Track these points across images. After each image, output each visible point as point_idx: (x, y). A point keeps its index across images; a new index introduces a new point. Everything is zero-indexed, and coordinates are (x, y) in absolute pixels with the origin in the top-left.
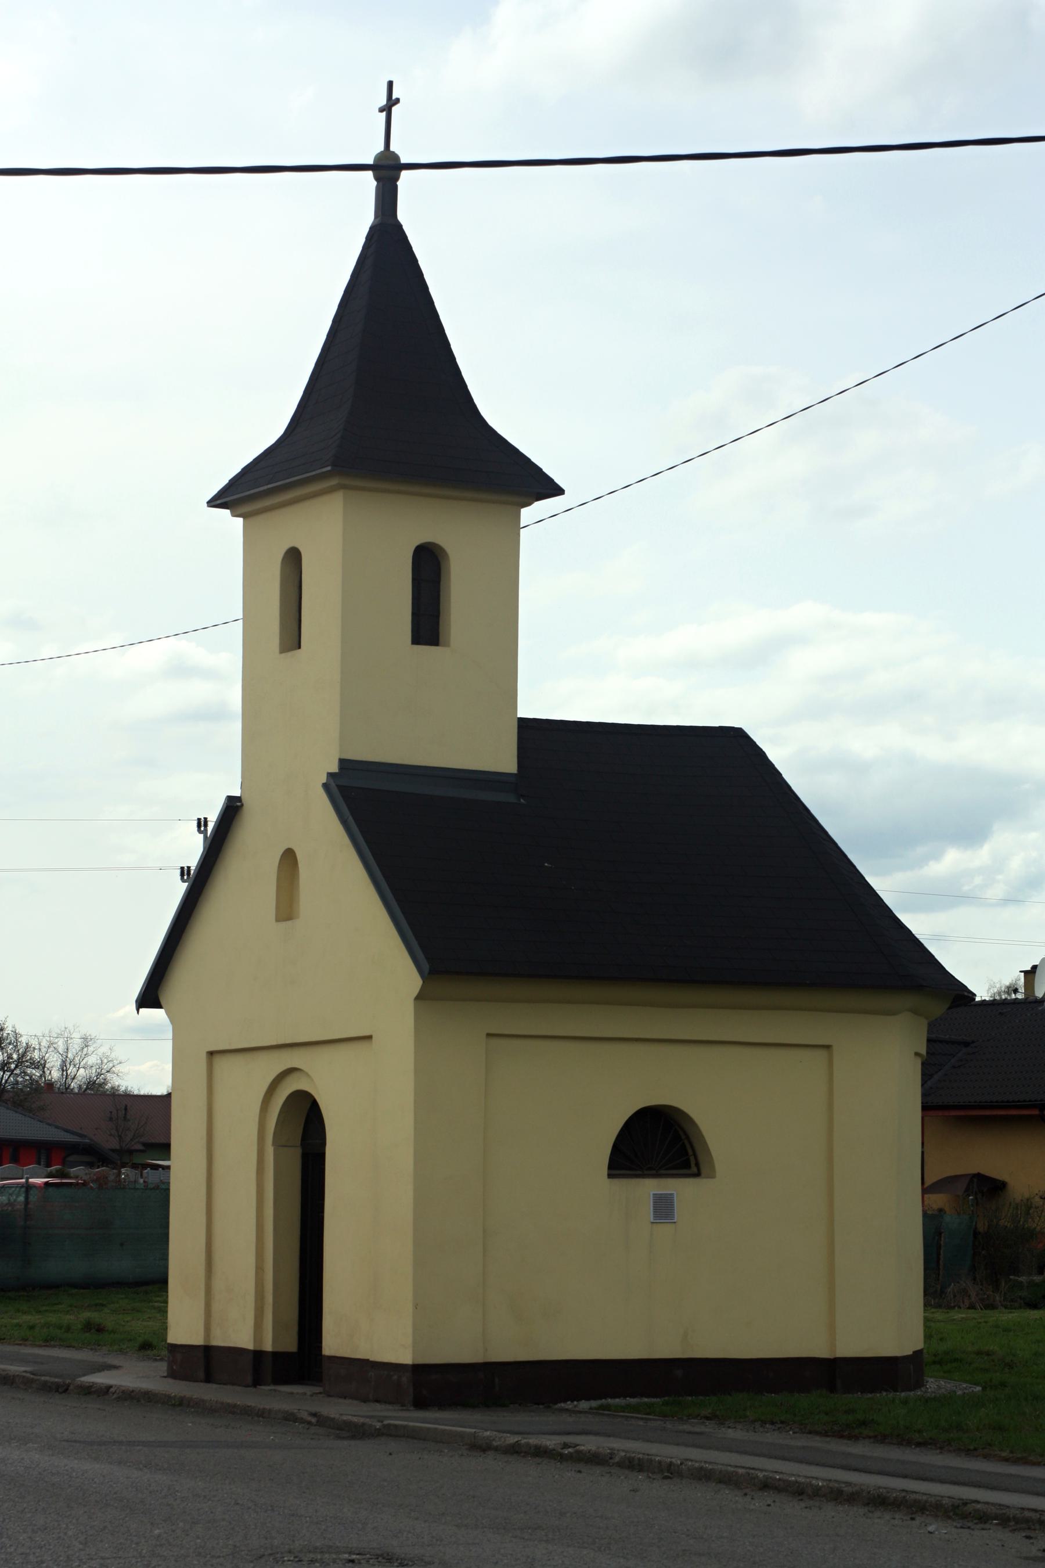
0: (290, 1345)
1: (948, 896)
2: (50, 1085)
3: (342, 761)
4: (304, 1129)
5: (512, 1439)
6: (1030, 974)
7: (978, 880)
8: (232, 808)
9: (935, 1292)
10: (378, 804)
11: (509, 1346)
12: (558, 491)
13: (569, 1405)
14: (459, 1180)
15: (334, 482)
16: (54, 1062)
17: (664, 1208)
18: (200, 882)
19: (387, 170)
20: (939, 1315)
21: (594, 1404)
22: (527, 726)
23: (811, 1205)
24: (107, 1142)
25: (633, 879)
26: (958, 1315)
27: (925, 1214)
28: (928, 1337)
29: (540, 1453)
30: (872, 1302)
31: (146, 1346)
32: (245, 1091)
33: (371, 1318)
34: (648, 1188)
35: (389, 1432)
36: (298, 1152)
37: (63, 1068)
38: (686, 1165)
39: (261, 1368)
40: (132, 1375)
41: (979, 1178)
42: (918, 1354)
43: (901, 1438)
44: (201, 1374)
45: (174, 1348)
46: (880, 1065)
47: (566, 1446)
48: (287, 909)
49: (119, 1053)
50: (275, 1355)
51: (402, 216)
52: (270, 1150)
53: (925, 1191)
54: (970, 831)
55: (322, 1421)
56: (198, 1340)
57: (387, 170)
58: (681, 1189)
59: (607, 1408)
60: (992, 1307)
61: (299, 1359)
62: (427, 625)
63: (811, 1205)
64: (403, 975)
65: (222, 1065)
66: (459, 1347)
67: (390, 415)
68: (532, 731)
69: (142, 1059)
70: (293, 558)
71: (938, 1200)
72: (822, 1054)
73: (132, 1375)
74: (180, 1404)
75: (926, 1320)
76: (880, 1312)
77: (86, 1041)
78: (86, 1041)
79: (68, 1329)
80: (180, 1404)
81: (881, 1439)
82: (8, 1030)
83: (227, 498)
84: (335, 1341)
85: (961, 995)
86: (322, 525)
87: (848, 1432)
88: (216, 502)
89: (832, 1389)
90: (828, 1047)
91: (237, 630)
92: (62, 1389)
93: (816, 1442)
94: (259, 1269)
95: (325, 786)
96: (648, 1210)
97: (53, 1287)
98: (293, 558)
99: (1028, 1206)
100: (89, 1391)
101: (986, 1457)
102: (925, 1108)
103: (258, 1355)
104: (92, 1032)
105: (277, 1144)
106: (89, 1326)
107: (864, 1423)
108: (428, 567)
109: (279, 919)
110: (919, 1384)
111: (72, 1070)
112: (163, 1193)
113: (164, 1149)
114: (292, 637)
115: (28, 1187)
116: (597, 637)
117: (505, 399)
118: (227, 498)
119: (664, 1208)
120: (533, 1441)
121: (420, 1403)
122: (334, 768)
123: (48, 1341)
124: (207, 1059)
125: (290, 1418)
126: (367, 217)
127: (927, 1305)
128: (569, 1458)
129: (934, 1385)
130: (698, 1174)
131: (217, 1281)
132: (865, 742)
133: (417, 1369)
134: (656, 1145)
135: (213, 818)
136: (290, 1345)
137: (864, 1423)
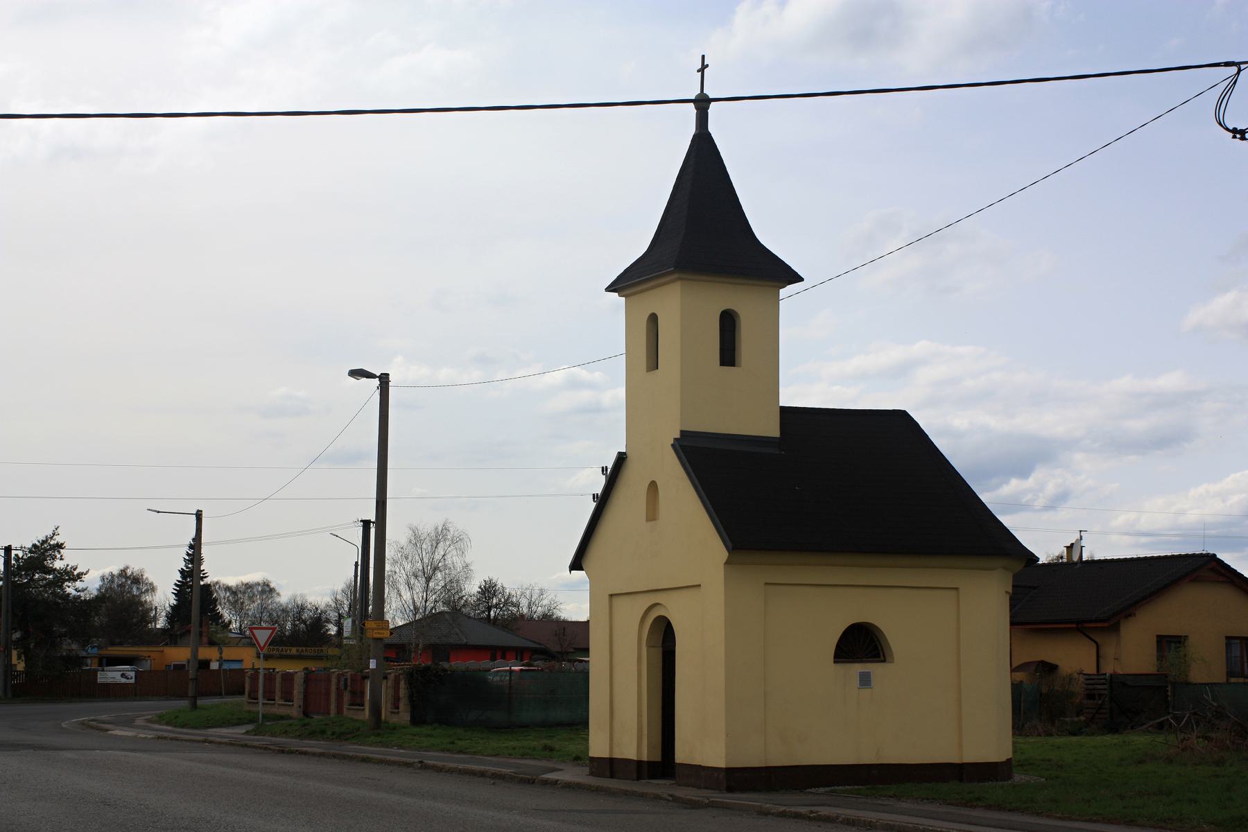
0: (657, 757)
1: (1016, 506)
2: (522, 616)
3: (682, 432)
4: (664, 638)
5: (782, 809)
6: (1070, 548)
7: (1029, 496)
8: (621, 459)
9: (1019, 727)
10: (704, 457)
11: (779, 757)
12: (800, 279)
13: (813, 790)
14: (753, 670)
15: (676, 276)
16: (524, 602)
17: (865, 680)
18: (603, 501)
19: (702, 103)
20: (1020, 740)
21: (827, 789)
22: (784, 410)
23: (948, 681)
24: (554, 648)
25: (847, 496)
26: (1031, 740)
27: (1012, 684)
28: (1014, 752)
29: (797, 816)
30: (987, 736)
31: (577, 758)
32: (630, 618)
33: (703, 742)
34: (857, 668)
35: (713, 805)
36: (660, 650)
37: (529, 607)
38: (878, 656)
39: (641, 770)
40: (569, 774)
41: (1043, 663)
42: (1009, 760)
43: (1000, 808)
44: (608, 774)
45: (592, 759)
46: (986, 599)
47: (812, 812)
48: (652, 515)
49: (560, 598)
50: (648, 762)
51: (712, 128)
52: (644, 649)
53: (1012, 671)
54: (1023, 471)
55: (676, 799)
56: (606, 755)
57: (702, 103)
58: (874, 669)
59: (835, 791)
60: (1051, 735)
61: (663, 765)
62: (728, 356)
63: (948, 681)
64: (718, 551)
65: (616, 601)
66: (752, 757)
67: (707, 241)
68: (789, 414)
69: (573, 601)
70: (653, 319)
71: (1020, 676)
72: (954, 592)
73: (569, 774)
74: (597, 790)
75: (1014, 743)
76: (987, 736)
77: (542, 592)
78: (542, 592)
79: (534, 749)
80: (597, 790)
81: (988, 807)
82: (499, 586)
83: (616, 287)
84: (683, 754)
85: (1033, 558)
86: (671, 300)
87: (969, 804)
88: (611, 288)
89: (961, 780)
90: (956, 589)
91: (622, 362)
92: (531, 782)
93: (952, 809)
94: (640, 715)
95: (673, 446)
96: (856, 681)
97: (525, 727)
98: (653, 319)
99: (1070, 678)
100: (546, 783)
101: (1048, 817)
102: (1012, 624)
103: (639, 763)
104: (546, 586)
105: (649, 646)
106: (545, 748)
107: (979, 799)
108: (728, 321)
109: (648, 520)
110: (1010, 777)
111: (534, 608)
112: (585, 675)
113: (586, 651)
114: (653, 363)
115: (511, 672)
116: (823, 362)
117: (770, 227)
118: (616, 287)
119: (865, 680)
120: (793, 809)
121: (730, 789)
122: (678, 436)
123: (523, 756)
124: (607, 599)
125: (657, 798)
126: (692, 130)
127: (1014, 734)
128: (814, 819)
129: (1018, 777)
130: (884, 661)
131: (616, 722)
132: (960, 421)
133: (729, 770)
134: (861, 644)
135: (610, 467)
136: (657, 757)
137: (979, 799)
